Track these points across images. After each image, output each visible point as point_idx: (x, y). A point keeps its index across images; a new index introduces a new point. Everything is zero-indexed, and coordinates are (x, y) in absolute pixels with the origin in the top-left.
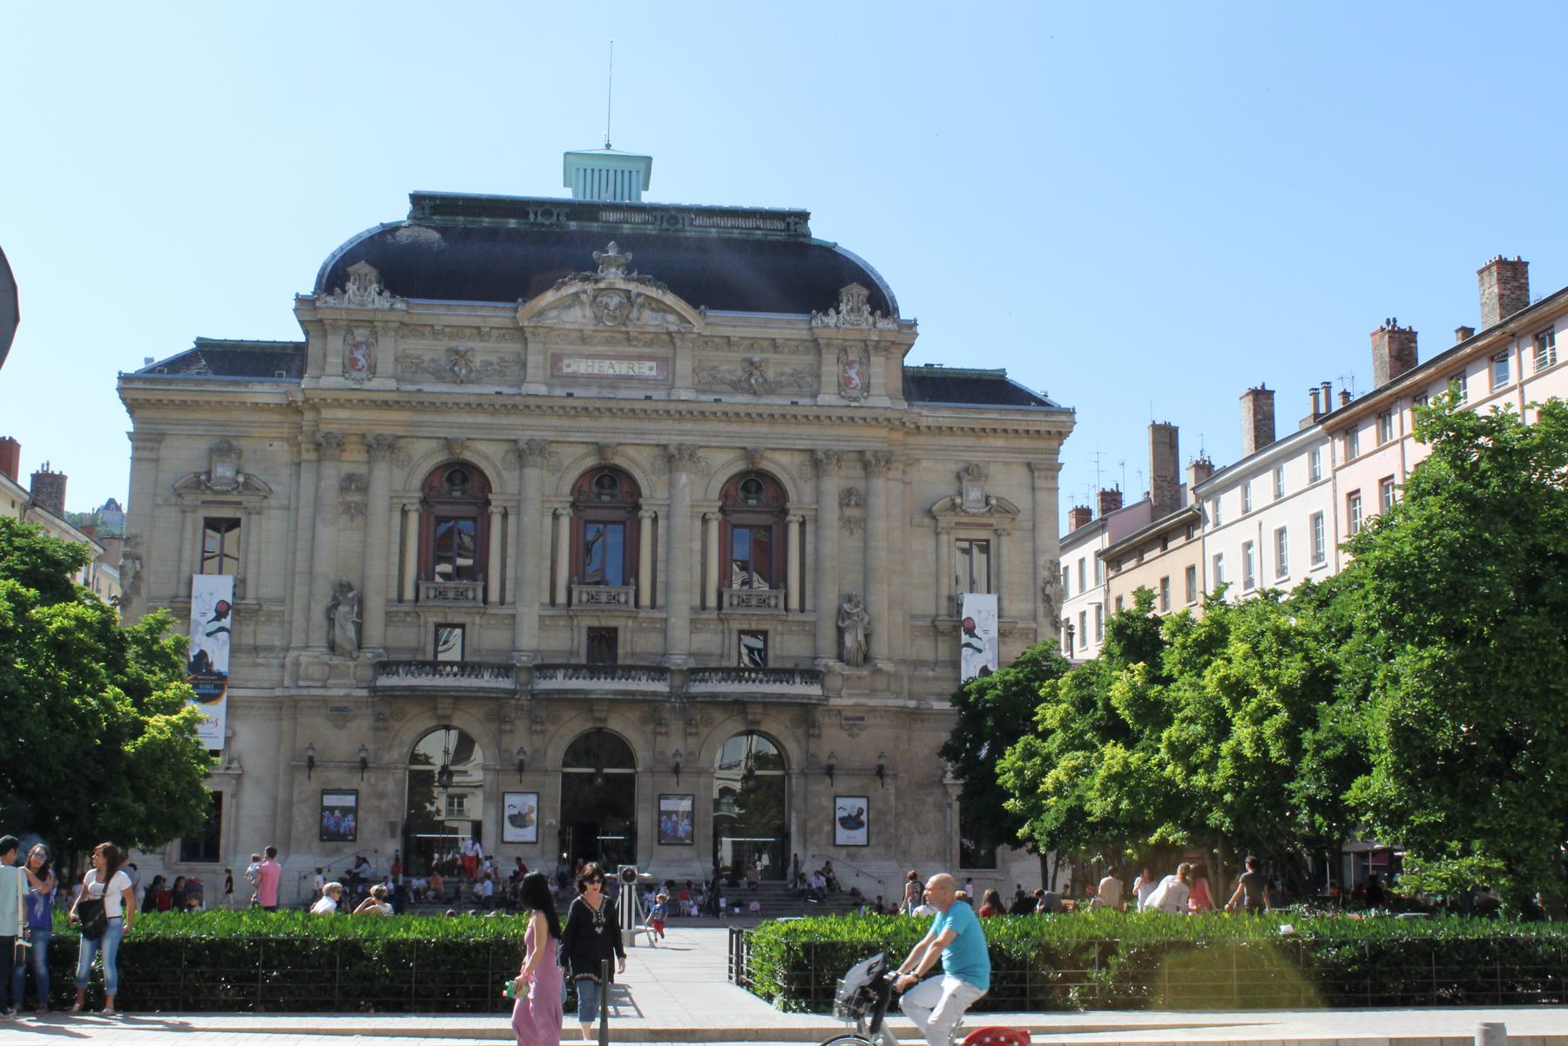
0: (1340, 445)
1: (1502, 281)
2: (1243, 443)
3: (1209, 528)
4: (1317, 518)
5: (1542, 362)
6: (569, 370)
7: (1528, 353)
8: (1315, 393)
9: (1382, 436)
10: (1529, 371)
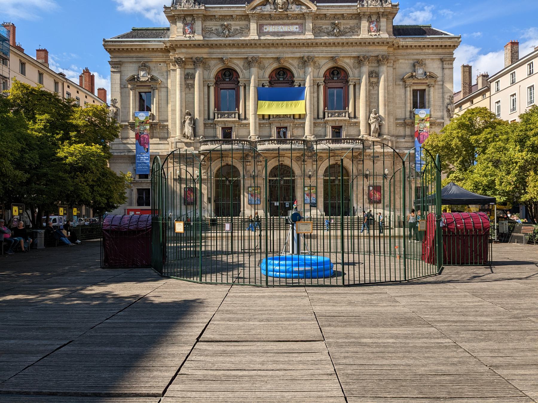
6: (266, 30)
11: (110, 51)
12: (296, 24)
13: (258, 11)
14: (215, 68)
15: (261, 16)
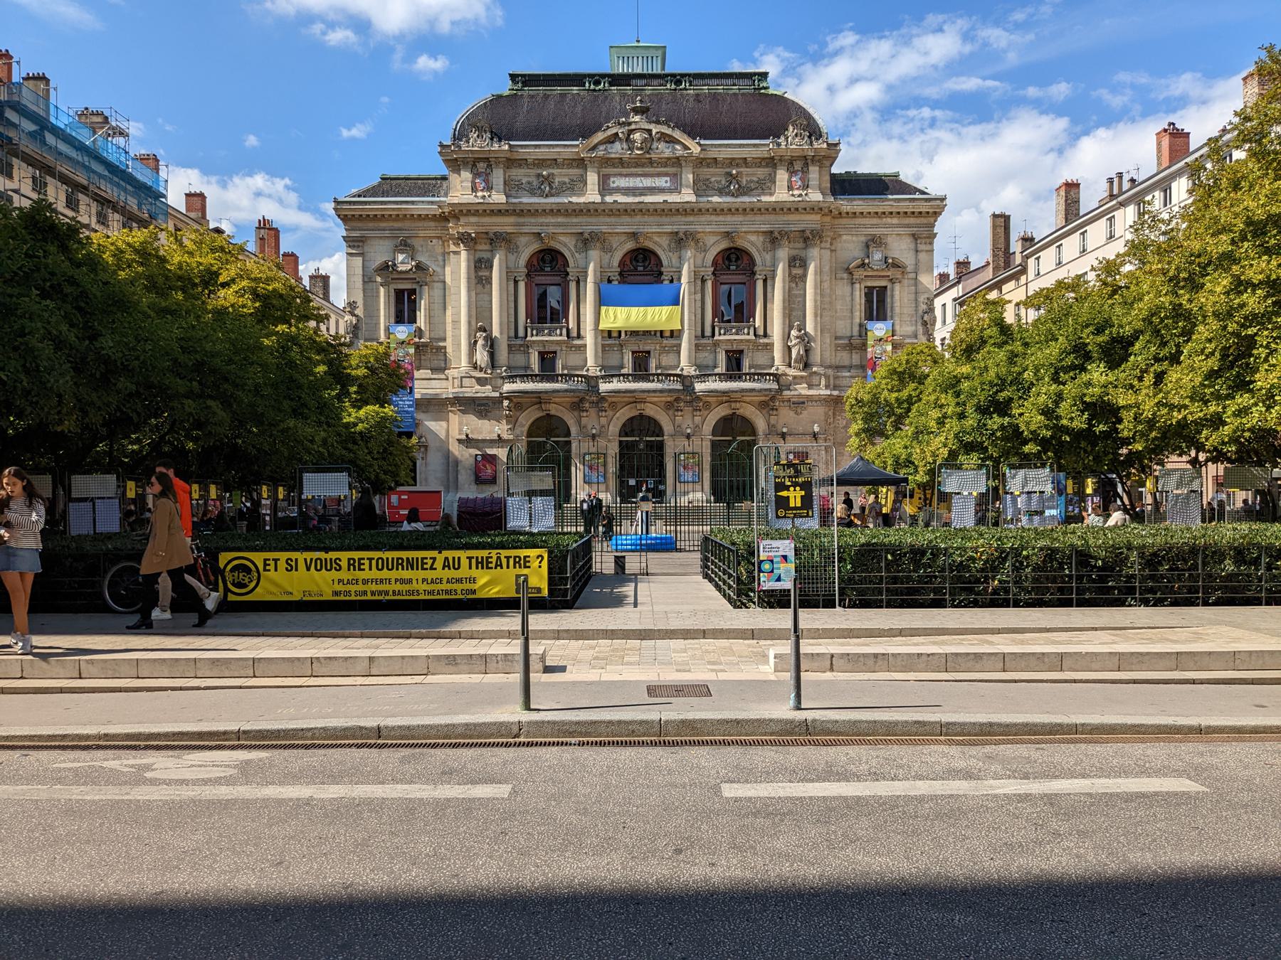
11: (345, 219)
12: (666, 175)
13: (601, 152)
14: (528, 249)
15: (607, 162)
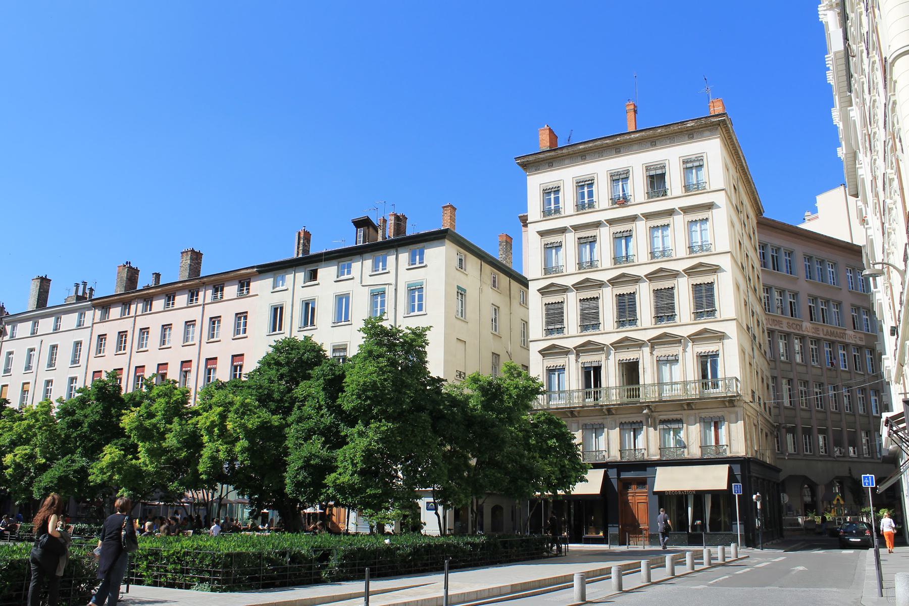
0: (98, 313)
1: (192, 259)
2: (31, 303)
3: (7, 338)
4: (78, 344)
5: (216, 298)
7: (209, 292)
8: (77, 285)
9: (123, 313)
10: (208, 300)
